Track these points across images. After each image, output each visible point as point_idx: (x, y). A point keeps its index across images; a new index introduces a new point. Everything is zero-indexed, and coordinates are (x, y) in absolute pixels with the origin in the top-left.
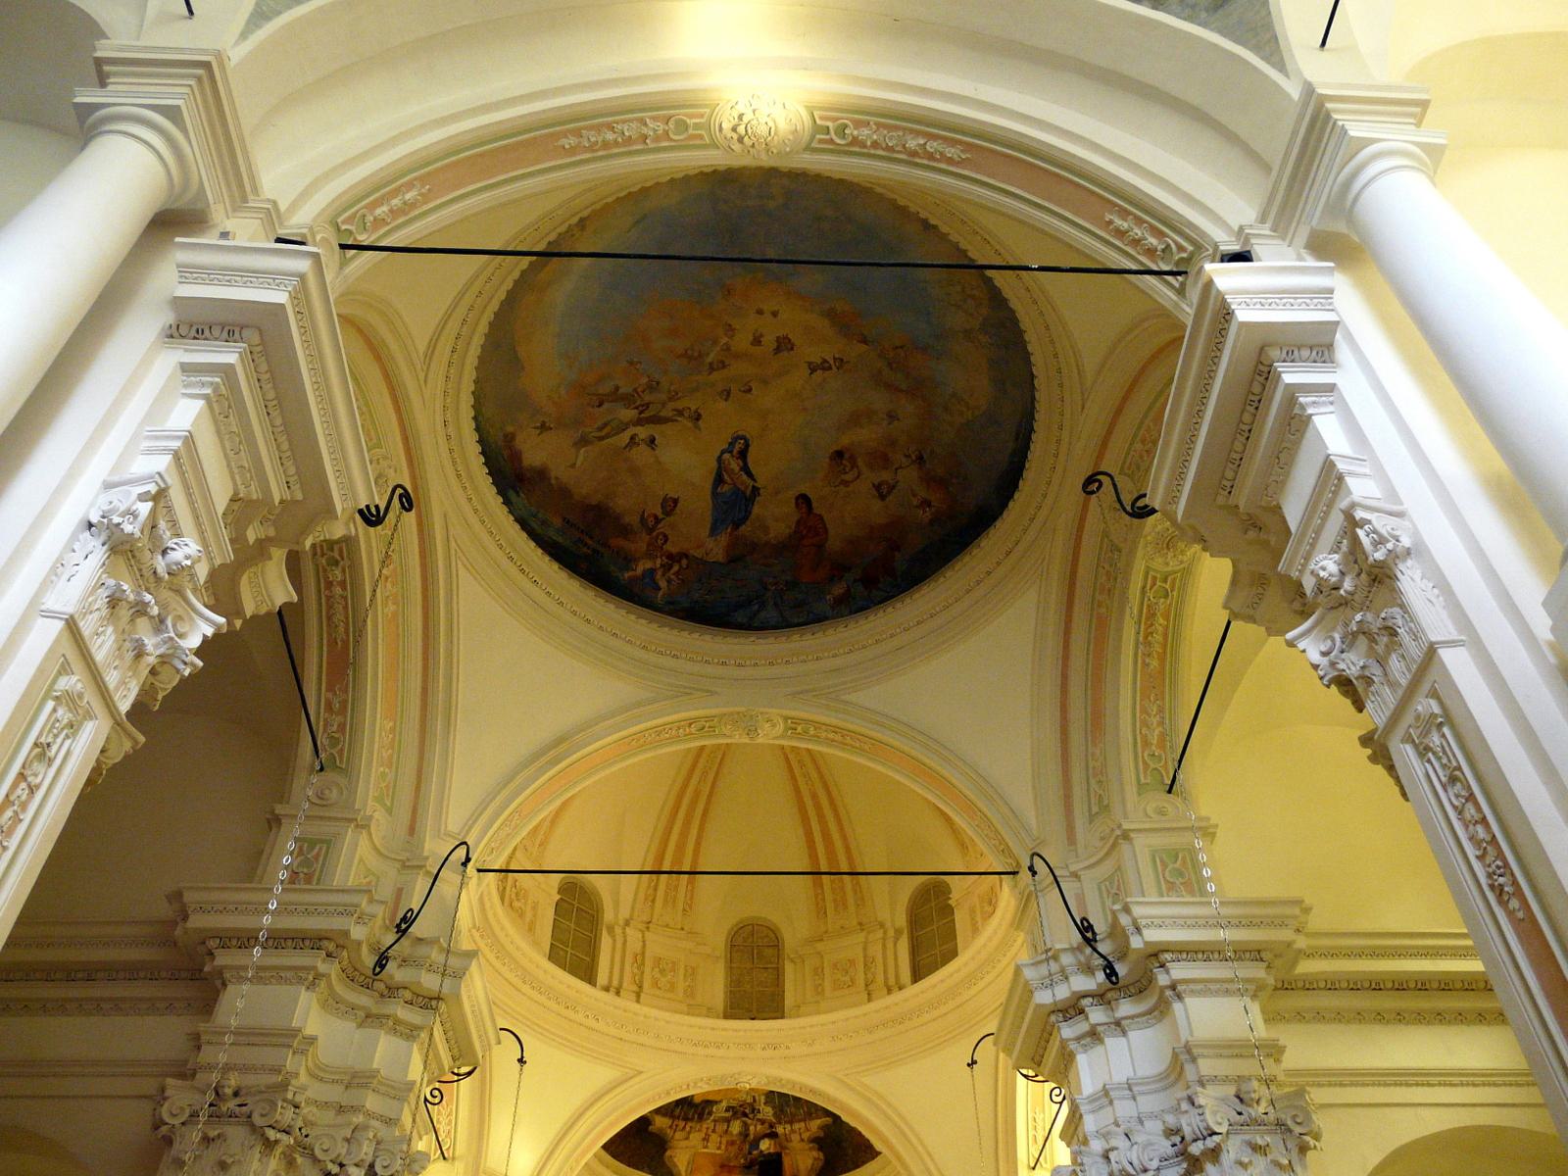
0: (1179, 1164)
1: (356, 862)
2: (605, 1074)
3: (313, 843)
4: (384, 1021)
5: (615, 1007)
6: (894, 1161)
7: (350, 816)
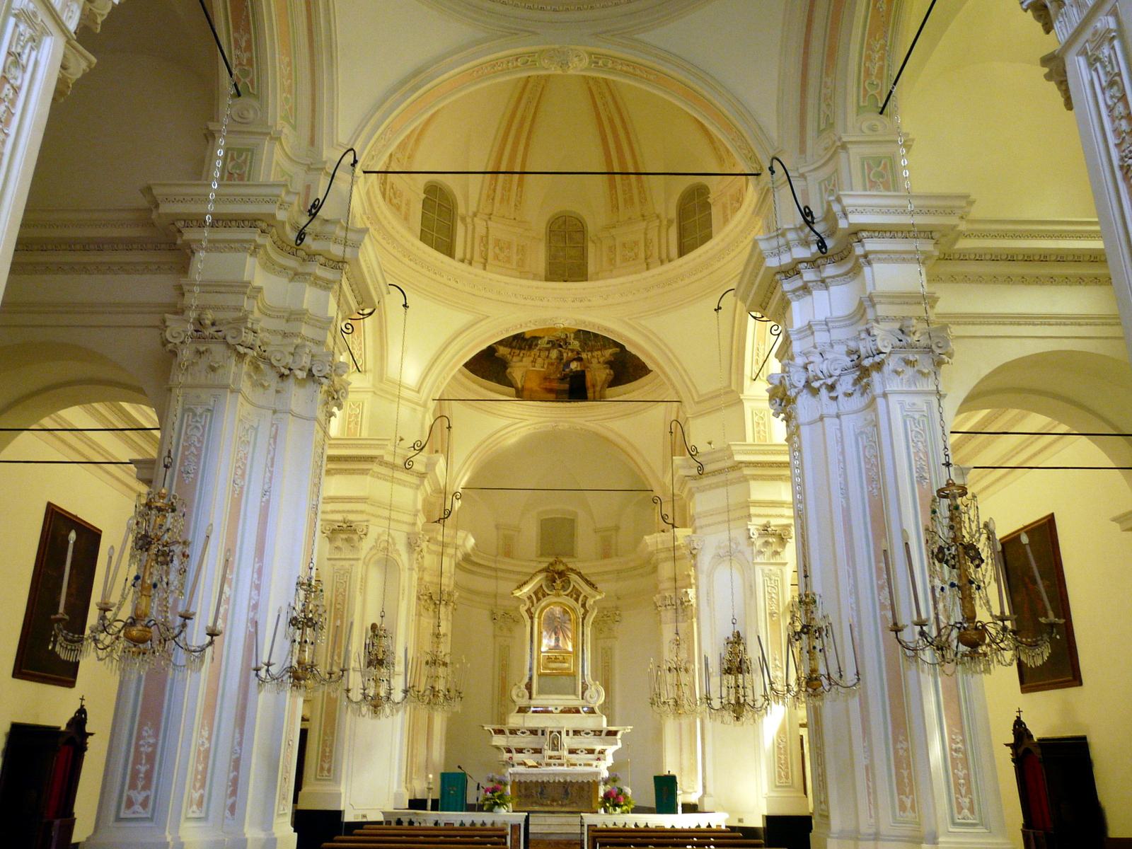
0: (854, 373)
1: (274, 164)
2: (460, 319)
3: (240, 152)
4: (307, 277)
5: (469, 273)
6: (662, 376)
7: (264, 131)
